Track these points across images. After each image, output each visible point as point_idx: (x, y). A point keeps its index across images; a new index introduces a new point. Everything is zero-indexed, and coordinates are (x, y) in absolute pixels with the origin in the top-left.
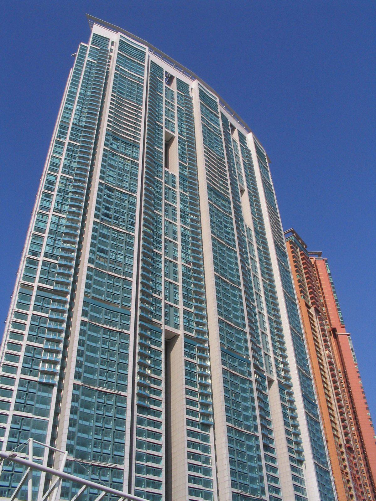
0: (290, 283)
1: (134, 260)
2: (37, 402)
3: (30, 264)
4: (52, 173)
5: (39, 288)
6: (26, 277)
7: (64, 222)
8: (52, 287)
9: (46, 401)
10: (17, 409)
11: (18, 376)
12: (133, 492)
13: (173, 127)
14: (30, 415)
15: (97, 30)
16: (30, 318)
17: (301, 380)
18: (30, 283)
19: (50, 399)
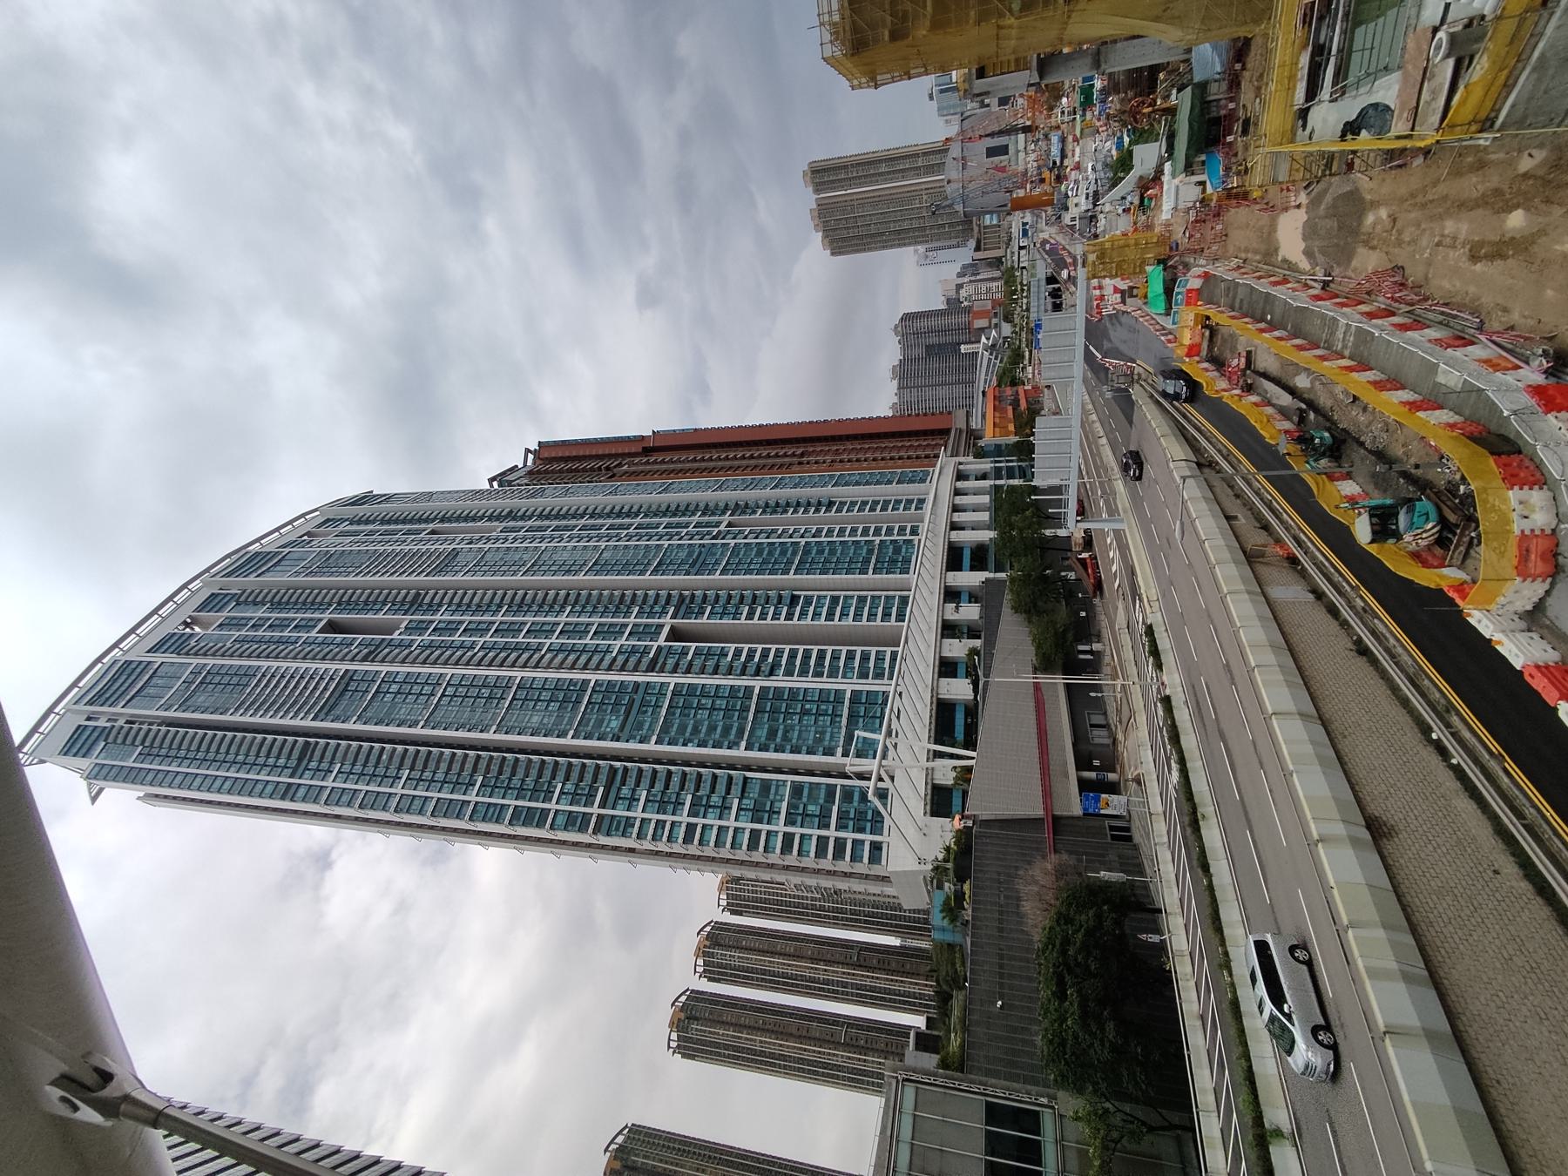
0: (1410, 208)
1: (931, 657)
2: (800, 799)
3: (519, 819)
4: (549, 821)
5: (603, 805)
6: (582, 829)
7: (569, 787)
8: (601, 789)
9: (766, 786)
10: (827, 826)
11: (832, 833)
12: (889, 682)
13: (688, 506)
14: (835, 809)
15: (1103, 796)
16: (841, 834)
17: (415, 500)
18: (594, 820)
19: (828, 785)
